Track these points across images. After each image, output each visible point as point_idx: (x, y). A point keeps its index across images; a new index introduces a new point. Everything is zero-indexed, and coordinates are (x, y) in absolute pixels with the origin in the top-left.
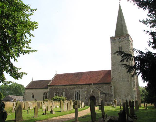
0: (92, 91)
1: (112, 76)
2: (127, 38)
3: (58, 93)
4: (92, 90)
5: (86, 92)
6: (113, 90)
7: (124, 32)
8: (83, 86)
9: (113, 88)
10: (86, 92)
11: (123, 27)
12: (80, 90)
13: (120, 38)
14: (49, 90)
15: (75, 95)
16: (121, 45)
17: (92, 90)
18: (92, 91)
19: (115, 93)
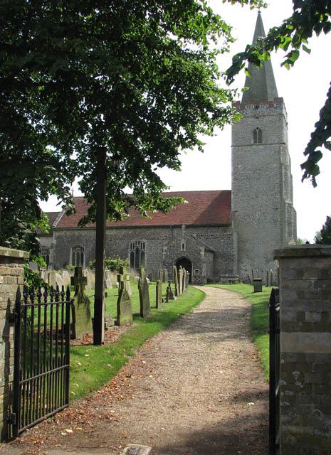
0: (183, 245)
1: (232, 207)
3: (82, 249)
4: (183, 242)
5: (165, 248)
6: (235, 245)
7: (269, 91)
8: (153, 230)
9: (235, 237)
10: (165, 248)
11: (267, 78)
12: (145, 241)
13: (257, 108)
14: (54, 242)
15: (129, 255)
17: (183, 242)
18: (183, 245)
19: (239, 250)
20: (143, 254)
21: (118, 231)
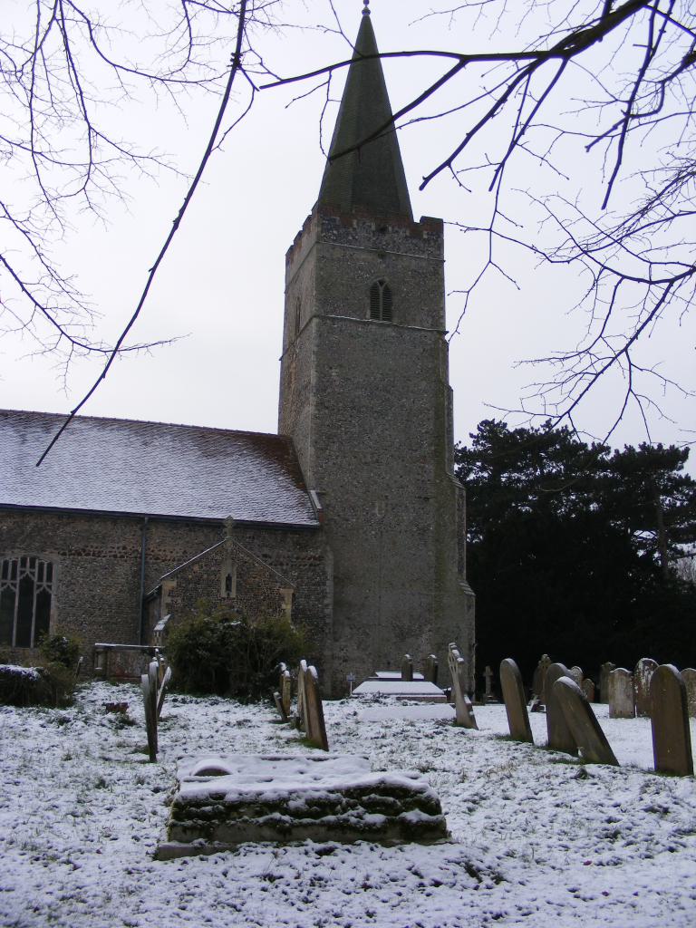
0: (229, 579)
2: (428, 241)
12: (56, 558)
16: (387, 279)
18: (229, 579)
20: (45, 599)
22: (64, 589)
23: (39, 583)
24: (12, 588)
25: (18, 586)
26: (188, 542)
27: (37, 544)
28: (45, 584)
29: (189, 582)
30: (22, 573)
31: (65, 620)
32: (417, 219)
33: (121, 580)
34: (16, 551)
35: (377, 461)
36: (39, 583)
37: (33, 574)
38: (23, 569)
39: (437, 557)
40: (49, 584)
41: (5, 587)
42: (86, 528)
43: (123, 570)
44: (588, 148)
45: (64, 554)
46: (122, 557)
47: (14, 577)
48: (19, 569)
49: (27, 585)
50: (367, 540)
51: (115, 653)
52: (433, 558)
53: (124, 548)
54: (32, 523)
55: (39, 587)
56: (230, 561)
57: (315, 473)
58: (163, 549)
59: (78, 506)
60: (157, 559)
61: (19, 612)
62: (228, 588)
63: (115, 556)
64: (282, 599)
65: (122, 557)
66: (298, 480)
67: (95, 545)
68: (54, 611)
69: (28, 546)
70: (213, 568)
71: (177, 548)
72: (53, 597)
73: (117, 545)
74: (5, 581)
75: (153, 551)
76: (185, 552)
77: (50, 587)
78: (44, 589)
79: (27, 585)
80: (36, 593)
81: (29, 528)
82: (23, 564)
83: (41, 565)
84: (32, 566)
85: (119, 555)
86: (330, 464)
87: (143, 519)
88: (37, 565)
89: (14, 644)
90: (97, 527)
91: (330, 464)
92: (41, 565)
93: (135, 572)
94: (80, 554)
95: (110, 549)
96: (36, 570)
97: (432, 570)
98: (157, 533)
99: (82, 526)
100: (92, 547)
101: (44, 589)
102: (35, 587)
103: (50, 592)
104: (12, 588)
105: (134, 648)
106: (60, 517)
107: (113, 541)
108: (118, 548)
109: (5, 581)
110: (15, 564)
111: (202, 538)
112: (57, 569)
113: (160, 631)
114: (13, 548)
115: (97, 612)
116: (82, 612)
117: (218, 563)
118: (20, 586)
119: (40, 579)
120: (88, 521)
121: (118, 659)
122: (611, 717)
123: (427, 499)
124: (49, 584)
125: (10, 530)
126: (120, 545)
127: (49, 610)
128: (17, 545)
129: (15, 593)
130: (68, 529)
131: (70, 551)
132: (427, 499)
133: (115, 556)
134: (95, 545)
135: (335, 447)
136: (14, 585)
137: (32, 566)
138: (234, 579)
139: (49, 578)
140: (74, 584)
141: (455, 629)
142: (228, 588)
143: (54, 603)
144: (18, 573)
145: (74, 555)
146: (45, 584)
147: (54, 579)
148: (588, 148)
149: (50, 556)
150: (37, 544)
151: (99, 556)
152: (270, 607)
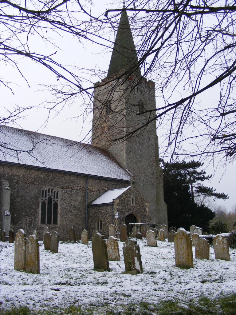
0: (133, 200)
12: (60, 190)
15: (40, 204)
18: (133, 200)
20: (56, 205)
21: (28, 172)
22: (62, 201)
23: (54, 199)
24: (45, 201)
25: (47, 200)
26: (99, 185)
27: (53, 184)
28: (56, 199)
29: (122, 200)
30: (48, 195)
31: (63, 213)
32: (148, 81)
33: (80, 199)
34: (47, 186)
35: (142, 161)
36: (54, 199)
37: (52, 195)
38: (49, 194)
39: (157, 193)
40: (57, 199)
41: (43, 200)
42: (69, 178)
43: (81, 194)
44: (18, 63)
45: (62, 188)
46: (80, 190)
47: (46, 197)
48: (47, 193)
49: (50, 200)
50: (140, 187)
51: (143, 226)
52: (156, 194)
53: (81, 187)
54: (51, 175)
55: (54, 200)
56: (133, 193)
57: (126, 163)
58: (92, 187)
59: (67, 170)
60: (90, 191)
61: (48, 210)
62: (133, 203)
63: (78, 190)
64: (146, 207)
65: (80, 190)
66: (119, 165)
67: (72, 185)
68: (59, 210)
69: (50, 184)
70: (128, 196)
71: (96, 187)
72: (59, 205)
73: (78, 186)
74: (42, 198)
75: (89, 188)
76: (98, 189)
77: (57, 201)
78: (44, 201)
79: (50, 200)
80: (53, 203)
81: (50, 177)
82: (49, 192)
83: (55, 192)
84: (52, 192)
85: (79, 189)
86: (130, 160)
87: (88, 176)
88: (53, 192)
89: (46, 223)
90: (72, 178)
91: (130, 160)
92: (55, 192)
93: (84, 196)
94: (67, 188)
95: (76, 187)
96: (53, 194)
97: (155, 198)
98: (90, 181)
99: (67, 178)
100: (71, 186)
101: (44, 201)
102: (53, 201)
103: (58, 203)
104: (45, 201)
105: (148, 225)
106: (60, 174)
107: (77, 184)
108: (79, 187)
109: (42, 198)
110: (46, 191)
111: (103, 184)
112: (60, 194)
113: (117, 218)
114: (46, 185)
115: (73, 211)
116: (68, 210)
117: (130, 194)
118: (48, 200)
119: (54, 198)
120: (69, 176)
121: (144, 229)
122: (168, 242)
123: (154, 174)
124: (57, 199)
125: (44, 178)
126: (79, 185)
127: (57, 210)
128: (47, 184)
129: (46, 203)
130: (63, 179)
131: (64, 187)
132: (154, 174)
133: (78, 190)
134: (72, 185)
135: (131, 155)
136: (46, 200)
137: (52, 192)
138: (134, 200)
139: (57, 198)
140: (65, 200)
141: (164, 217)
142: (133, 203)
143: (59, 207)
144: (47, 195)
145: (65, 188)
146: (56, 199)
147: (59, 198)
148: (18, 63)
149: (57, 189)
150: (53, 184)
151: (73, 189)
152: (143, 210)
